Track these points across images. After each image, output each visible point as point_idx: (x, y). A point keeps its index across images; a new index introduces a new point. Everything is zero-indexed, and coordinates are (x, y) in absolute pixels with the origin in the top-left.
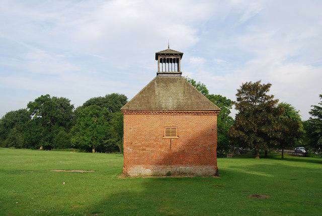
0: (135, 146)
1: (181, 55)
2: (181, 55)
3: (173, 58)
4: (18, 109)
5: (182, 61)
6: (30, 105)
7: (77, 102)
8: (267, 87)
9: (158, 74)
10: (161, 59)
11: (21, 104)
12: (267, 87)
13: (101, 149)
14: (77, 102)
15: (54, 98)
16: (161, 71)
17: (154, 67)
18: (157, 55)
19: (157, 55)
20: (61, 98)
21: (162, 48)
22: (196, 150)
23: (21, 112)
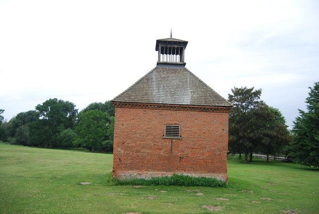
0: (128, 147)
1: (185, 43)
2: (185, 43)
3: (176, 46)
4: (27, 111)
5: (187, 51)
6: (38, 108)
7: (81, 106)
8: (258, 93)
9: (158, 64)
10: (162, 48)
11: (30, 106)
12: (258, 93)
13: (92, 147)
14: (81, 106)
15: (60, 101)
16: (161, 61)
17: (150, 59)
18: (159, 42)
19: (159, 42)
20: (67, 102)
21: (165, 36)
22: (203, 154)
23: (30, 113)
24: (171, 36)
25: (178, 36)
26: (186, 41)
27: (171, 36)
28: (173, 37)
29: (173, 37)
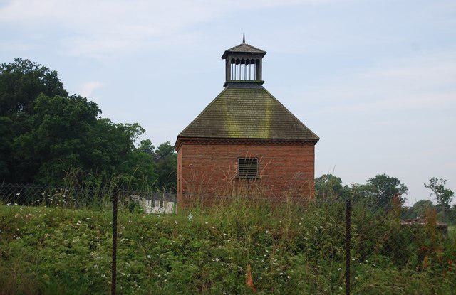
1: (263, 54)
5: (264, 60)
9: (229, 83)
16: (253, 66)
21: (233, 43)
24: (244, 41)
25: (256, 43)
26: (264, 50)
27: (244, 41)
28: (246, 43)
29: (246, 43)
